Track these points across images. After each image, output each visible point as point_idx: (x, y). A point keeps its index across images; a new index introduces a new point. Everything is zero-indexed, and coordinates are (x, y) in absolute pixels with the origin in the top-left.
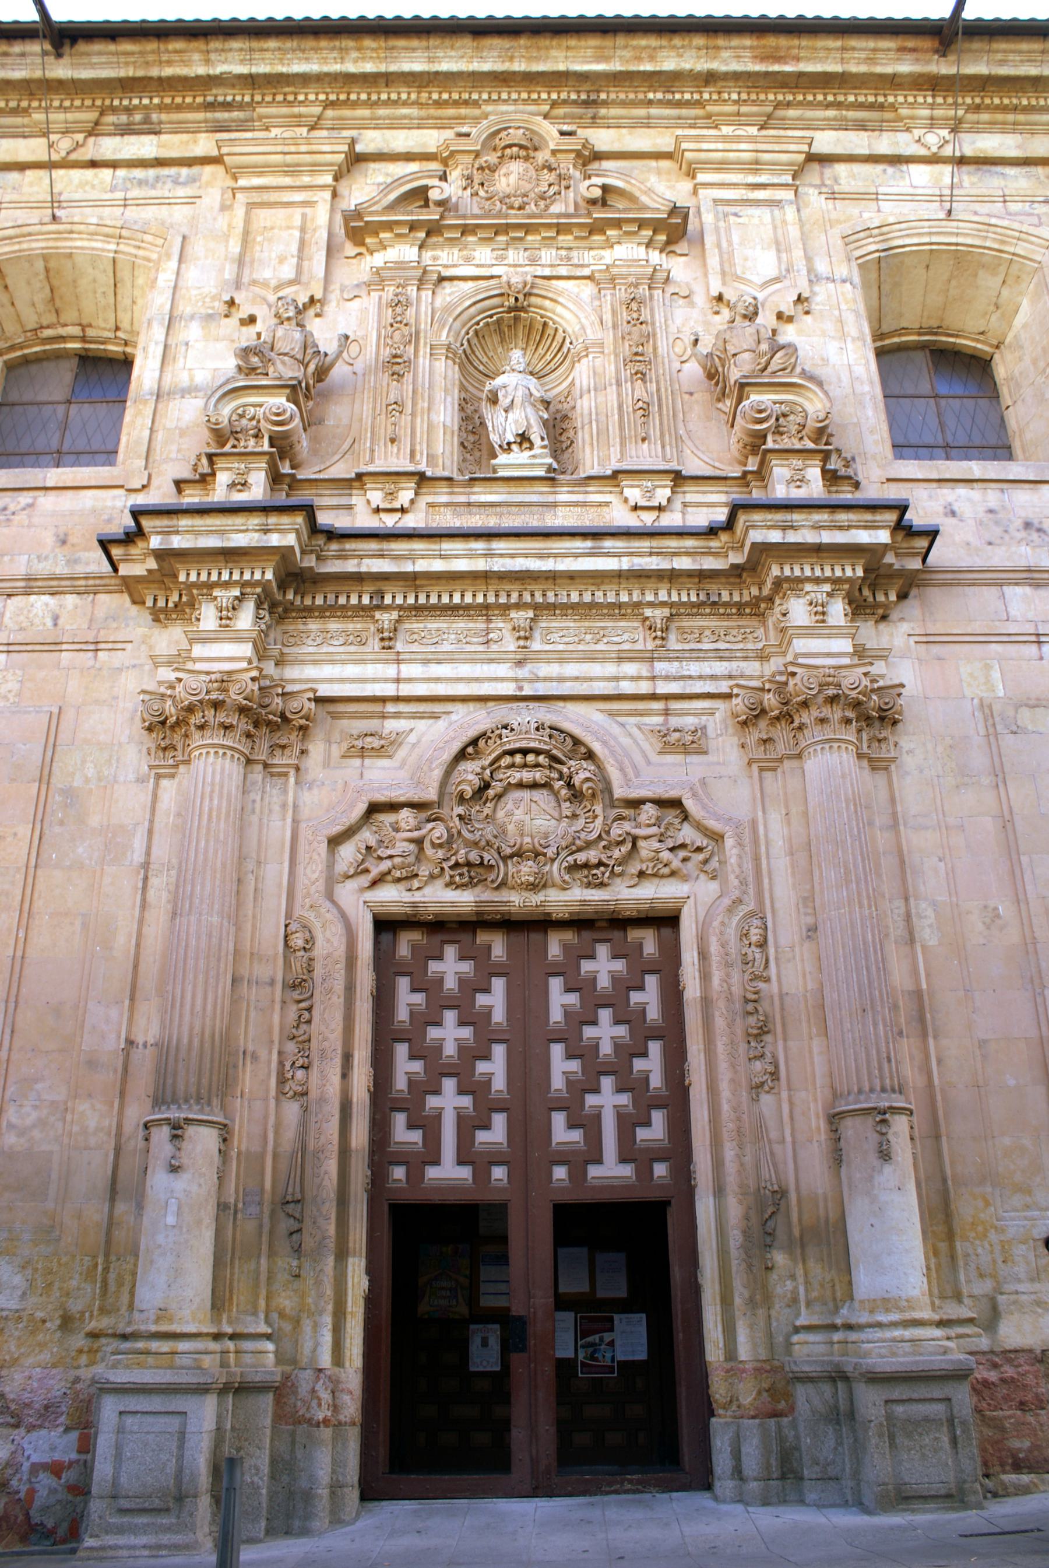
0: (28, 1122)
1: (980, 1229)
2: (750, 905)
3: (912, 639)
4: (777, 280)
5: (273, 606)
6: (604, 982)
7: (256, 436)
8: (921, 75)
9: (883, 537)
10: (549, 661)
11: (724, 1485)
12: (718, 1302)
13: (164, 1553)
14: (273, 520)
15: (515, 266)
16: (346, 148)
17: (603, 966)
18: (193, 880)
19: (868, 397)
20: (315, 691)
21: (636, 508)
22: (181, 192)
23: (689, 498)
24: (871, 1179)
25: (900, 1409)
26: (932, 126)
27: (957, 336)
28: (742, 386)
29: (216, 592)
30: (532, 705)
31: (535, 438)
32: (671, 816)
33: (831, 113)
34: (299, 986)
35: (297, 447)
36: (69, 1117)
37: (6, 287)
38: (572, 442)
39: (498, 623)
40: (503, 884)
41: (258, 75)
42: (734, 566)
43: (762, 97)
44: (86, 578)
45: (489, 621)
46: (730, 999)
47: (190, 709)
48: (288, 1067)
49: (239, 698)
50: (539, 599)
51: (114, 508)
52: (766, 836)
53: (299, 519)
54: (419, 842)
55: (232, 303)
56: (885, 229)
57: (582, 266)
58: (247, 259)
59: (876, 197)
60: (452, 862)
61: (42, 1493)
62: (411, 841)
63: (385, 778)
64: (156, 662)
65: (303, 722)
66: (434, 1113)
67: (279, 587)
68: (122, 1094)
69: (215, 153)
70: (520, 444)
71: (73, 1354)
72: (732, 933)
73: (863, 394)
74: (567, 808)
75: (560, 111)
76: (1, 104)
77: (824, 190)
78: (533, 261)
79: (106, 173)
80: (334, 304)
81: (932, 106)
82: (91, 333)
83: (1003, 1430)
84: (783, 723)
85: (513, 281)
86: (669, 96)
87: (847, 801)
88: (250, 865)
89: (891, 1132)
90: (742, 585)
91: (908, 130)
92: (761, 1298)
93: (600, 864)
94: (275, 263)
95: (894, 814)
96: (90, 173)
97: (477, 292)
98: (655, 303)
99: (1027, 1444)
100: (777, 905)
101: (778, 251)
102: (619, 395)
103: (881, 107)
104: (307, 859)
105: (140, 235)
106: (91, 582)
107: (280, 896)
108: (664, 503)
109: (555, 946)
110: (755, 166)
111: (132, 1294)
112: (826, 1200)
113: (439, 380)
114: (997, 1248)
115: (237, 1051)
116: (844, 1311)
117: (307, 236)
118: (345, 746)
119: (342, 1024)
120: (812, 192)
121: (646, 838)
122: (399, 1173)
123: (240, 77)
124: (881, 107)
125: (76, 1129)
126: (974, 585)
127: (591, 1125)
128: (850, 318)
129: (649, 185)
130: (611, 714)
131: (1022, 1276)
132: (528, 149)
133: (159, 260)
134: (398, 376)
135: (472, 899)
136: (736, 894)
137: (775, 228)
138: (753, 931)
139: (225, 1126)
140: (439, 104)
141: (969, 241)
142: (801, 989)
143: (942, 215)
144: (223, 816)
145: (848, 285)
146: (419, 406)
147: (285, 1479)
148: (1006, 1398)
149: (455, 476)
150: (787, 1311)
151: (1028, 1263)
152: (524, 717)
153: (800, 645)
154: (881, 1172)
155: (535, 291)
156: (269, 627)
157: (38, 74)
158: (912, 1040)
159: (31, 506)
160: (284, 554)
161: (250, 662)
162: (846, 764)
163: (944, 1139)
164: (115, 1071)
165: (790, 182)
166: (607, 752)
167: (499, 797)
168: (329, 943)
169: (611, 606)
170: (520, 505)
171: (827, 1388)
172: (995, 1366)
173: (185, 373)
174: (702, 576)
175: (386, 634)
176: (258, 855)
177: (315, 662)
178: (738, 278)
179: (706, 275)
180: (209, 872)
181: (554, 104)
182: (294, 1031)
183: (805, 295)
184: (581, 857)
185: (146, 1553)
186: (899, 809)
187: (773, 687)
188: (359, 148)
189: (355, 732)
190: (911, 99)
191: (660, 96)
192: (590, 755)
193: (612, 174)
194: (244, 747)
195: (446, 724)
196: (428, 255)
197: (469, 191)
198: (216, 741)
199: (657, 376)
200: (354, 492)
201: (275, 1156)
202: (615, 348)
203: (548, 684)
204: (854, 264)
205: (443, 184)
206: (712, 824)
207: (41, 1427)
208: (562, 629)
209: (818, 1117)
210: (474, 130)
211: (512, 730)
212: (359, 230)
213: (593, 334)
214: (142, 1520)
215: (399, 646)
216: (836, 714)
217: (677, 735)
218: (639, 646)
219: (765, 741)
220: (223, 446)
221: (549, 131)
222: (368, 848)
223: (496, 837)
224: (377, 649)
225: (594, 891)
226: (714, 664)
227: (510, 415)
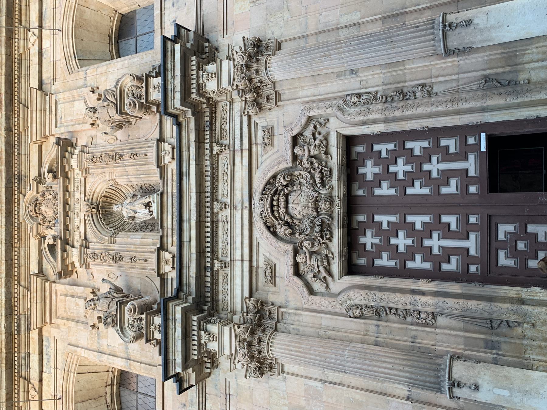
5: (211, 315)
8: (6, 43)
9: (178, 47)
10: (234, 195)
15: (80, 209)
17: (369, 170)
18: (328, 363)
19: (129, 61)
29: (202, 342)
31: (147, 200)
33: (23, 80)
34: (379, 313)
35: (147, 301)
38: (150, 185)
43: (16, 109)
46: (385, 109)
47: (252, 357)
48: (419, 321)
52: (309, 97)
53: (171, 305)
54: (311, 254)
55: (93, 326)
56: (67, 58)
57: (80, 181)
58: (77, 319)
59: (55, 62)
62: (311, 258)
63: (284, 267)
66: (441, 250)
67: (202, 313)
69: (37, 330)
72: (354, 110)
73: (128, 63)
75: (23, 190)
76: (34, 407)
77: (52, 83)
78: (79, 201)
80: (95, 283)
82: (109, 382)
85: (86, 210)
86: (16, 146)
87: (292, 58)
88: (322, 332)
90: (204, 113)
93: (321, 172)
95: (300, 38)
98: (94, 151)
100: (341, 89)
101: (74, 101)
102: (129, 166)
104: (319, 308)
105: (68, 363)
106: (201, 395)
107: (337, 319)
108: (170, 146)
110: (43, 111)
113: (124, 240)
115: (412, 346)
119: (396, 295)
120: (53, 88)
124: (20, 60)
128: (100, 70)
130: (257, 168)
132: (36, 203)
134: (121, 258)
135: (337, 230)
137: (66, 102)
138: (353, 100)
139: (451, 357)
140: (20, 239)
144: (299, 345)
145: (87, 71)
149: (160, 234)
153: (225, 84)
154: (477, 25)
155: (90, 201)
156: (219, 318)
157: (4, 404)
158: (406, 20)
160: (185, 312)
162: (276, 60)
167: (291, 217)
168: (359, 297)
175: (223, 265)
176: (318, 328)
177: (234, 297)
180: (325, 355)
182: (401, 317)
184: (318, 180)
186: (297, 36)
187: (244, 96)
188: (37, 272)
189: (265, 280)
192: (274, 177)
195: (261, 240)
196: (77, 245)
198: (266, 346)
199: (122, 150)
201: (466, 331)
202: (111, 167)
204: (80, 69)
205: (47, 238)
206: (303, 122)
208: (222, 189)
209: (446, 62)
212: (66, 272)
215: (228, 260)
216: (255, 66)
217: (266, 139)
218: (228, 156)
219: (268, 99)
221: (31, 194)
222: (314, 277)
223: (309, 219)
225: (334, 175)
226: (235, 121)
227: (138, 211)
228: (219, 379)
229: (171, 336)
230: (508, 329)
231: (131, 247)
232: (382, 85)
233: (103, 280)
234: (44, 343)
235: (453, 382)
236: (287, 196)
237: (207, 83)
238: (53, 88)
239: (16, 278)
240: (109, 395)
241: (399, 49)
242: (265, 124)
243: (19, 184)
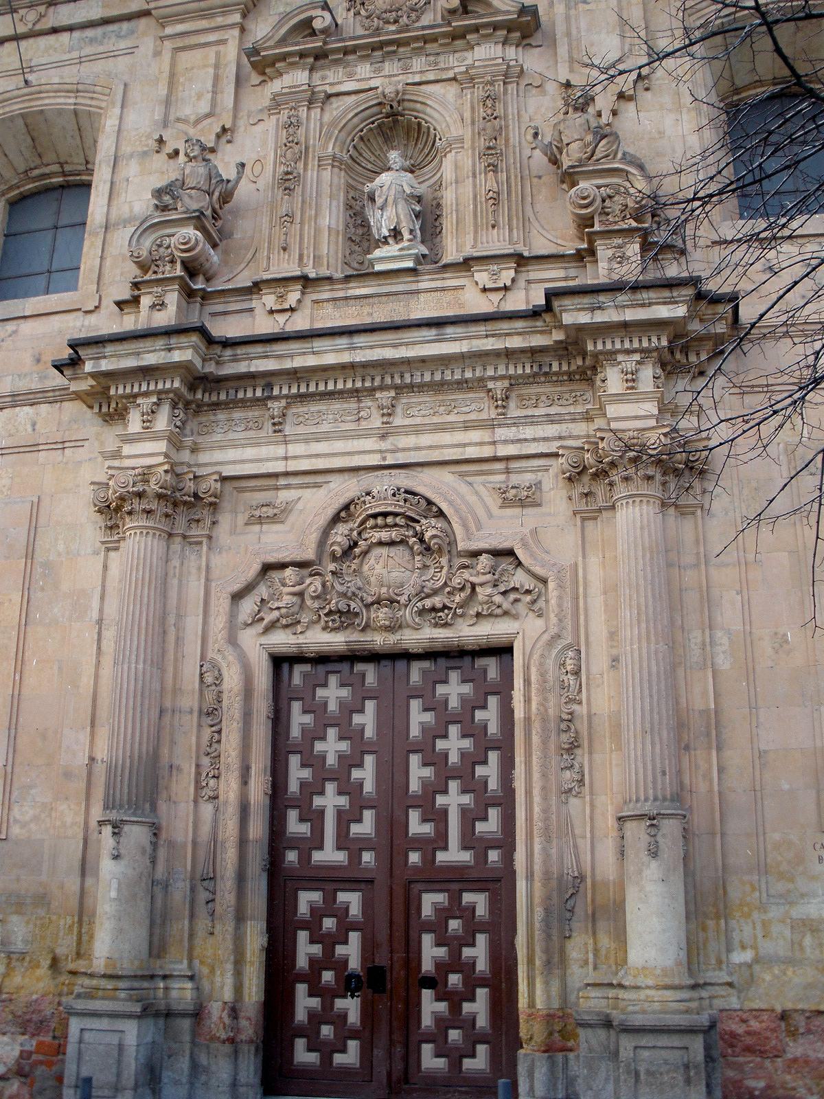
0: (27, 818)
5: (187, 404)
14: (174, 340)
15: (390, 76)
17: (454, 690)
20: (220, 474)
22: (123, 44)
24: (640, 872)
29: (139, 401)
30: (393, 472)
32: (505, 564)
34: (211, 714)
36: (54, 814)
39: (367, 402)
44: (53, 391)
45: (359, 401)
46: (544, 720)
47: (122, 499)
50: (398, 381)
51: (74, 327)
52: (585, 578)
54: (301, 594)
55: (161, 141)
58: (173, 98)
65: (213, 499)
72: (550, 663)
78: (406, 70)
79: (65, 37)
80: (242, 129)
82: (67, 168)
85: (387, 91)
93: (445, 607)
96: (52, 39)
97: (358, 104)
99: (762, 1084)
100: (592, 639)
102: (475, 186)
106: (57, 393)
108: (508, 283)
109: (416, 672)
112: (614, 883)
113: (326, 189)
117: (221, 71)
118: (247, 516)
121: (481, 585)
122: (292, 856)
125: (58, 823)
130: (462, 475)
133: (107, 106)
135: (343, 639)
136: (553, 630)
138: (569, 662)
152: (383, 484)
155: (407, 97)
156: (184, 423)
159: (15, 332)
160: (184, 368)
162: (645, 515)
166: (452, 511)
168: (232, 681)
169: (458, 382)
170: (387, 294)
172: (744, 1021)
174: (533, 352)
175: (276, 420)
177: (221, 448)
184: (428, 603)
189: (254, 503)
192: (441, 514)
194: (164, 525)
196: (317, 76)
211: (373, 497)
212: (262, 64)
213: (455, 131)
215: (288, 429)
217: (513, 492)
218: (484, 416)
219: (586, 495)
222: (263, 600)
224: (270, 431)
225: (440, 630)
226: (546, 428)
228: (85, 426)
229: (142, 345)
233: (243, 165)
234: (125, 26)
240: (46, 170)
242: (546, 486)
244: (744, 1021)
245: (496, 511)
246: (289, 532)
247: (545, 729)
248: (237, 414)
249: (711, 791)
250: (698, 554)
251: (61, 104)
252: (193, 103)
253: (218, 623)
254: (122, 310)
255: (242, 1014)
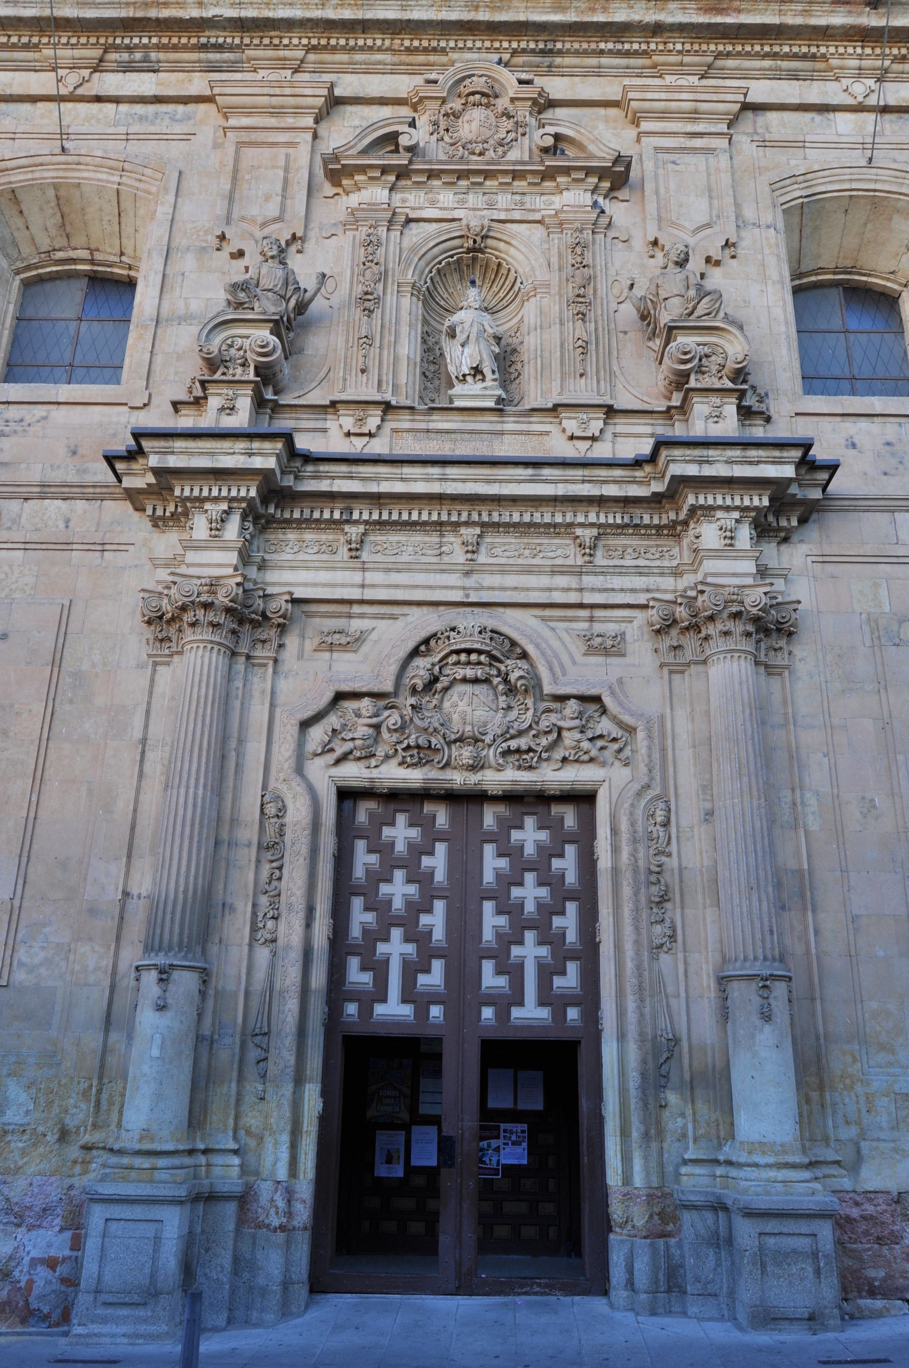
0: (36, 961)
1: (848, 1081)
2: (656, 790)
3: (810, 559)
4: (708, 225)
5: (257, 518)
6: (530, 850)
7: (243, 365)
8: (853, 27)
9: (788, 471)
10: (492, 573)
11: (619, 1294)
12: (618, 1133)
13: (141, 1341)
15: (474, 209)
16: (325, 92)
17: (530, 836)
19: (784, 336)
20: (291, 594)
21: (572, 438)
23: (619, 429)
24: (753, 1036)
25: (771, 1241)
26: (860, 76)
27: (869, 275)
28: (671, 329)
29: (208, 506)
30: (477, 610)
31: (487, 371)
32: (592, 708)
33: (767, 63)
34: (271, 847)
35: (280, 376)
36: (72, 957)
37: (21, 212)
38: (519, 374)
39: (450, 538)
40: (447, 765)
41: (247, 19)
42: (655, 494)
43: (704, 47)
45: (442, 536)
46: (636, 871)
47: (183, 608)
48: (260, 919)
49: (226, 600)
50: (485, 518)
52: (673, 730)
53: (279, 445)
54: (377, 727)
55: (222, 237)
56: (809, 176)
57: (533, 210)
58: (237, 196)
59: (802, 145)
60: (405, 745)
61: (39, 1283)
62: (370, 726)
64: (155, 563)
65: (281, 620)
66: (384, 957)
68: (118, 938)
69: (208, 92)
70: (474, 376)
71: (69, 1164)
72: (639, 812)
74: (502, 701)
75: (519, 60)
77: (756, 138)
78: (491, 206)
79: (110, 107)
81: (860, 57)
82: (98, 256)
83: (862, 1261)
84: (692, 632)
85: (472, 224)
89: (772, 996)
91: (837, 79)
92: (654, 1132)
93: (530, 750)
94: (260, 203)
96: (95, 107)
97: (440, 234)
98: (597, 247)
99: (882, 1274)
100: (680, 791)
101: (710, 197)
102: (561, 333)
103: (814, 57)
105: (140, 169)
106: (98, 490)
108: (597, 434)
109: (490, 817)
110: (694, 115)
111: (121, 1112)
112: (713, 1049)
113: (405, 317)
114: (862, 1100)
116: (726, 1149)
117: (290, 175)
118: (317, 641)
121: (569, 729)
122: (351, 1009)
123: (230, 20)
124: (814, 57)
126: (868, 511)
127: (515, 972)
128: (772, 261)
129: (596, 133)
130: (544, 619)
131: (884, 1124)
132: (489, 96)
136: (646, 780)
137: (709, 175)
138: (659, 813)
139: (205, 969)
140: (410, 51)
141: (887, 188)
142: (698, 865)
143: (864, 163)
146: (386, 340)
147: (246, 1275)
148: (866, 1233)
149: (416, 405)
150: (677, 1144)
151: (889, 1114)
152: (469, 621)
154: (762, 1030)
155: (491, 234)
156: (252, 536)
157: (47, 13)
159: (45, 418)
160: (265, 475)
161: (236, 569)
162: (743, 671)
163: (818, 1002)
164: (113, 918)
165: (726, 131)
166: (539, 654)
167: (446, 689)
168: (298, 812)
169: (548, 525)
170: (471, 432)
171: (709, 1216)
172: (857, 1204)
173: (180, 305)
174: (627, 502)
175: (353, 546)
177: (292, 568)
178: (674, 224)
179: (644, 220)
181: (515, 53)
182: (267, 886)
183: (732, 241)
184: (513, 744)
185: (126, 1341)
187: (684, 601)
188: (338, 92)
189: (326, 630)
190: (841, 50)
191: (610, 46)
192: (524, 655)
193: (564, 121)
196: (397, 197)
197: (435, 136)
200: (329, 417)
202: (560, 289)
203: (491, 592)
204: (779, 210)
205: (412, 130)
207: (39, 1226)
208: (504, 544)
210: (441, 77)
211: (459, 632)
212: (337, 172)
213: (542, 275)
214: (124, 1312)
215: (365, 556)
216: (738, 628)
217: (599, 640)
218: (570, 562)
219: (675, 648)
220: (215, 373)
221: (508, 79)
222: (334, 731)
223: (442, 725)
224: (346, 558)
225: (524, 773)
226: (640, 575)
227: (466, 350)
230: (255, 1061)
231: (390, 334)
232: (680, 865)
235: (165, 972)
236: (487, 681)
237: (715, 526)
238: (742, 140)
239: (323, 42)
241: (737, 901)
242: (628, 637)
243: (533, 51)
244: (857, 1204)
245: (579, 658)
246: (363, 662)
247: (636, 880)
248: (309, 536)
249: (808, 952)
250: (786, 714)
251: (101, 180)
252: (260, 203)
253: (284, 751)
254: (177, 411)
255: (296, 1196)
